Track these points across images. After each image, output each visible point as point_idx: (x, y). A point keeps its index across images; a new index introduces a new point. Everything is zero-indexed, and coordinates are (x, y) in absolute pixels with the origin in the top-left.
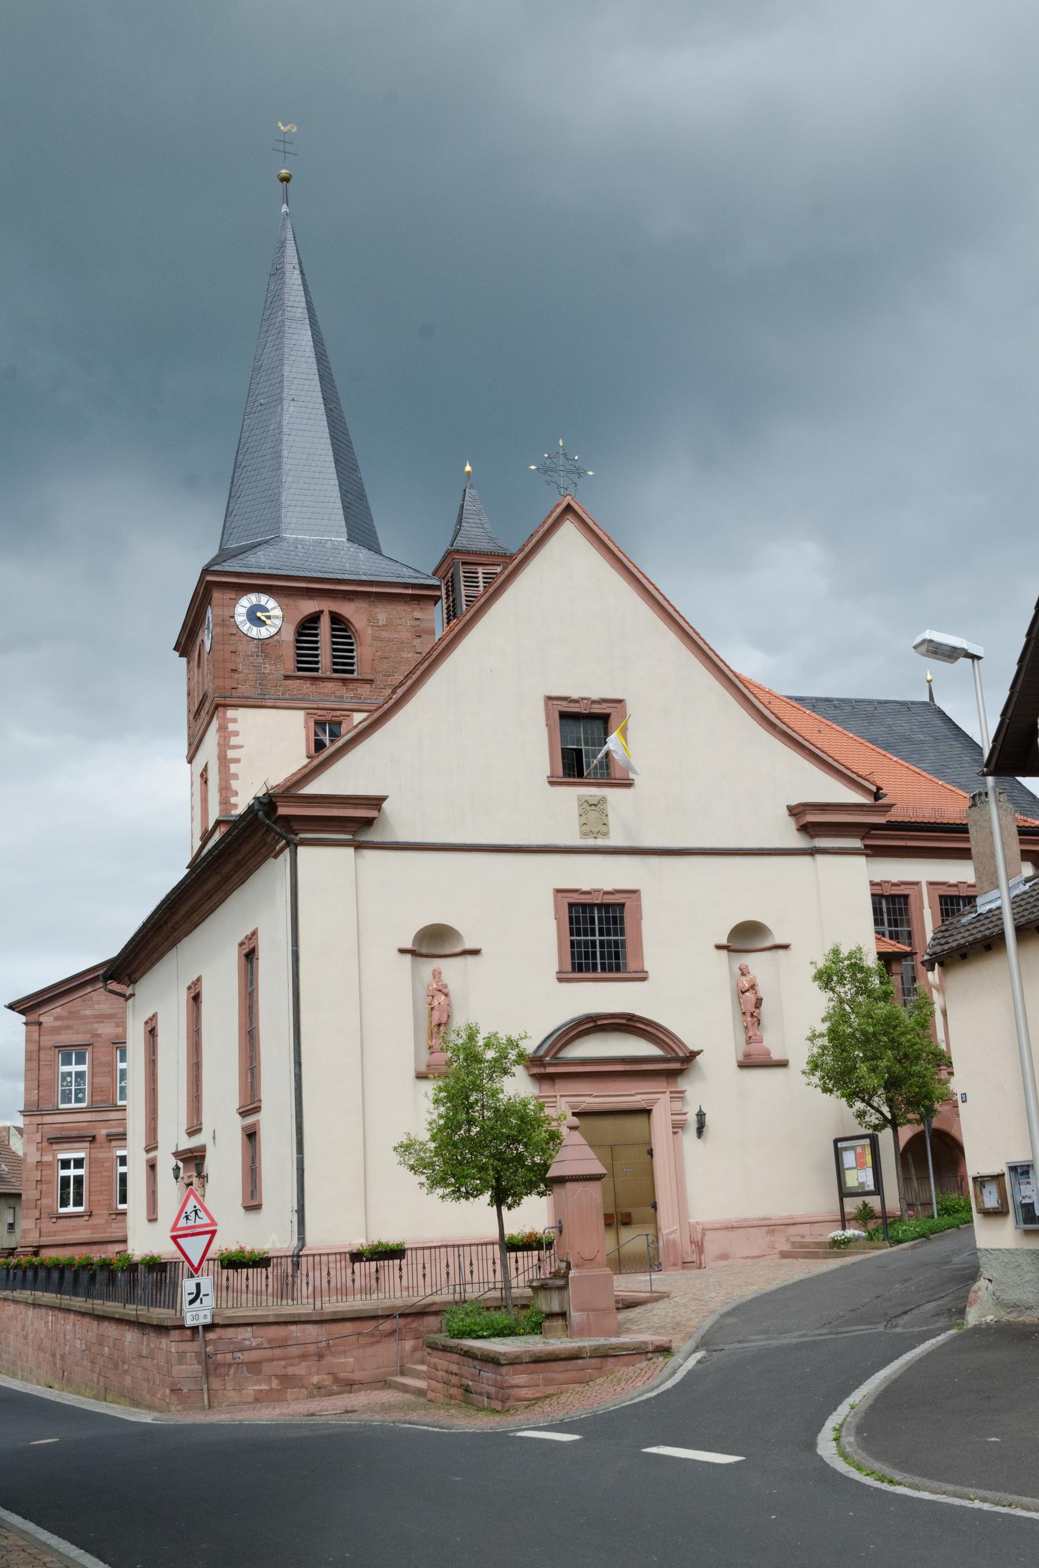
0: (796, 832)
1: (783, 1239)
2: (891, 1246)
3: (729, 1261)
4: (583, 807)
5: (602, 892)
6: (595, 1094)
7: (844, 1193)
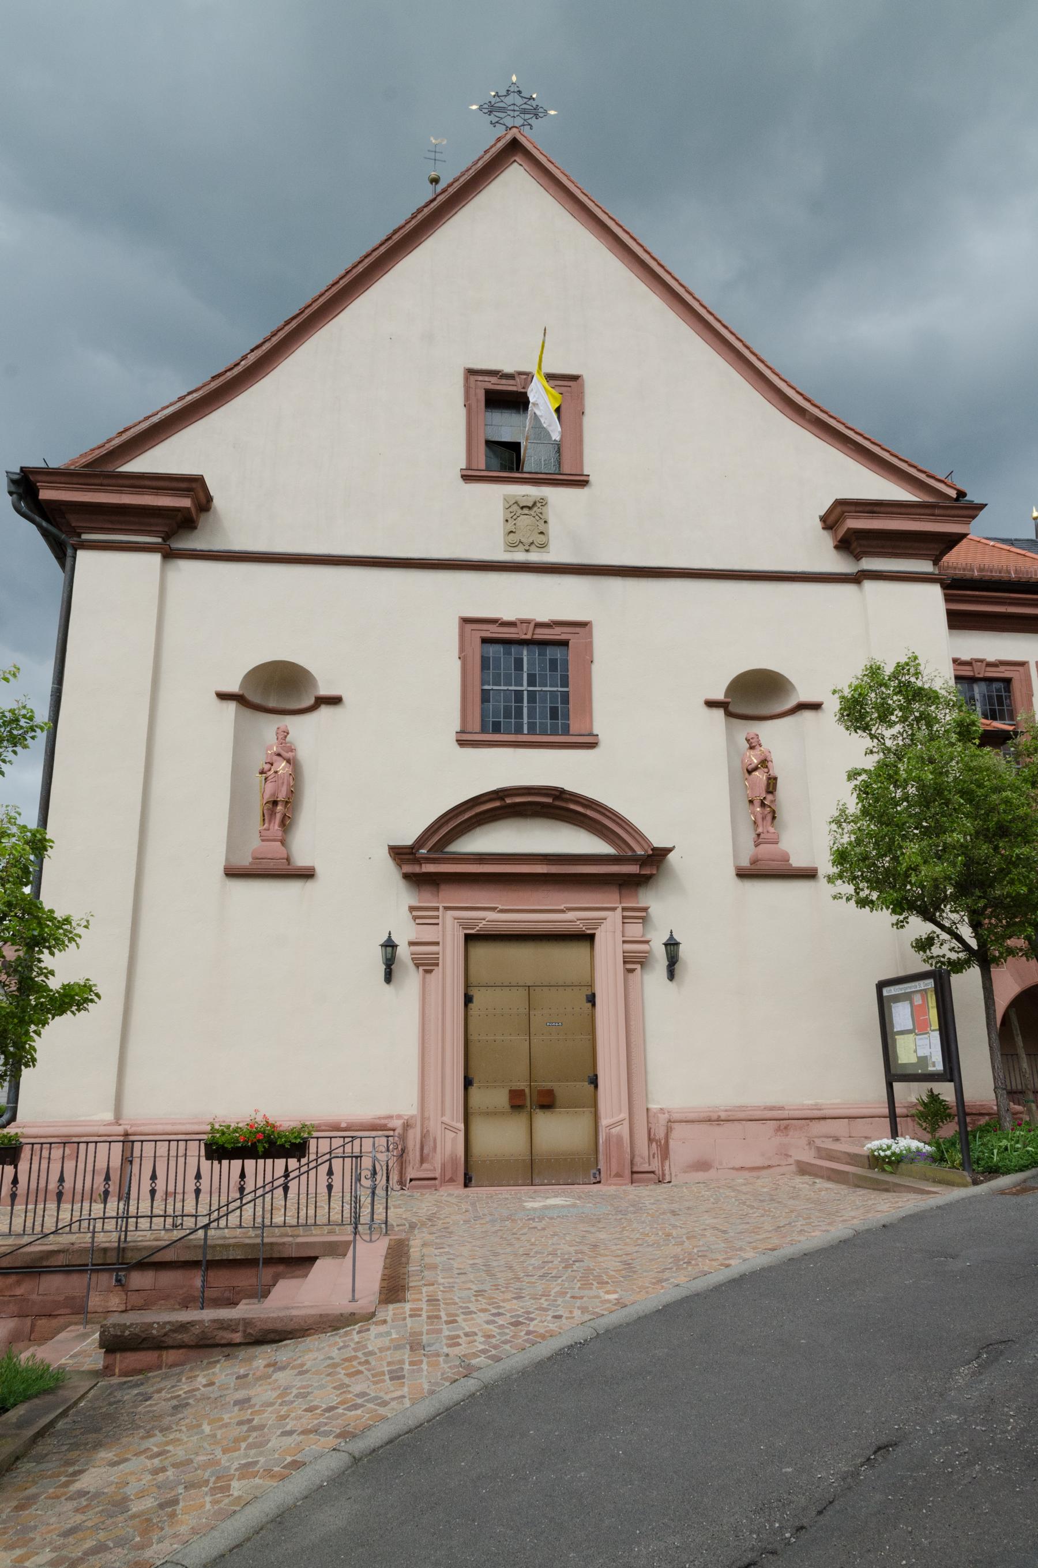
0: (833, 552)
1: (803, 1141)
2: (975, 1183)
3: (712, 1174)
4: (511, 510)
5: (532, 626)
6: (501, 907)
7: (894, 1074)
